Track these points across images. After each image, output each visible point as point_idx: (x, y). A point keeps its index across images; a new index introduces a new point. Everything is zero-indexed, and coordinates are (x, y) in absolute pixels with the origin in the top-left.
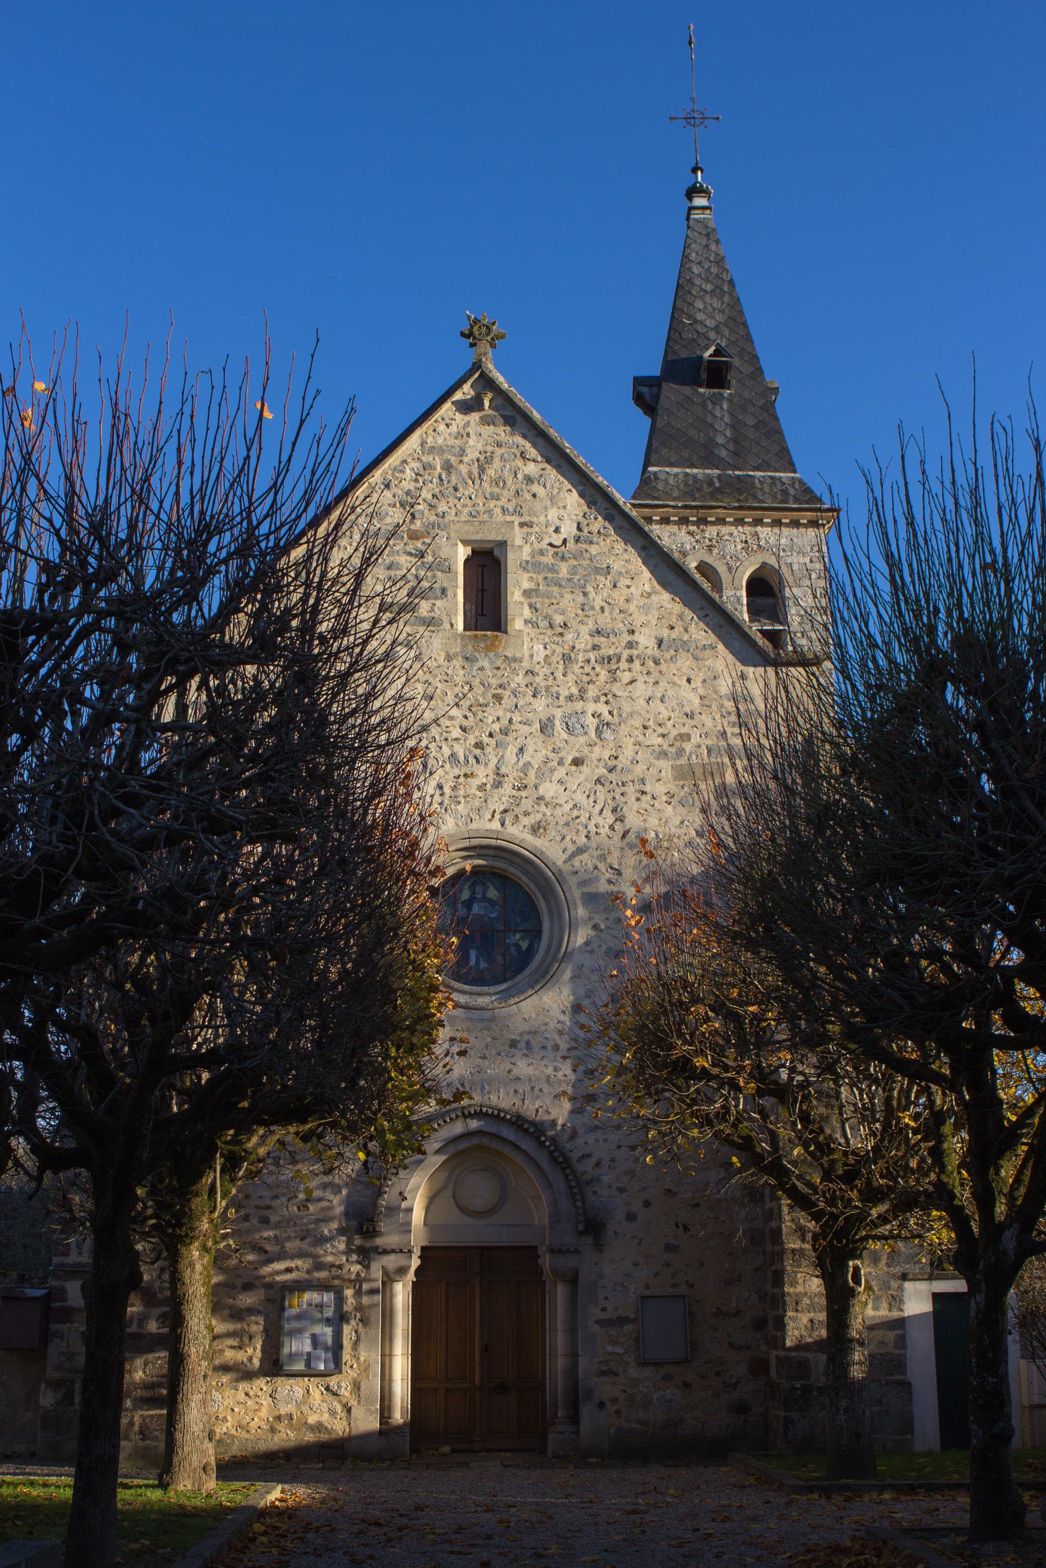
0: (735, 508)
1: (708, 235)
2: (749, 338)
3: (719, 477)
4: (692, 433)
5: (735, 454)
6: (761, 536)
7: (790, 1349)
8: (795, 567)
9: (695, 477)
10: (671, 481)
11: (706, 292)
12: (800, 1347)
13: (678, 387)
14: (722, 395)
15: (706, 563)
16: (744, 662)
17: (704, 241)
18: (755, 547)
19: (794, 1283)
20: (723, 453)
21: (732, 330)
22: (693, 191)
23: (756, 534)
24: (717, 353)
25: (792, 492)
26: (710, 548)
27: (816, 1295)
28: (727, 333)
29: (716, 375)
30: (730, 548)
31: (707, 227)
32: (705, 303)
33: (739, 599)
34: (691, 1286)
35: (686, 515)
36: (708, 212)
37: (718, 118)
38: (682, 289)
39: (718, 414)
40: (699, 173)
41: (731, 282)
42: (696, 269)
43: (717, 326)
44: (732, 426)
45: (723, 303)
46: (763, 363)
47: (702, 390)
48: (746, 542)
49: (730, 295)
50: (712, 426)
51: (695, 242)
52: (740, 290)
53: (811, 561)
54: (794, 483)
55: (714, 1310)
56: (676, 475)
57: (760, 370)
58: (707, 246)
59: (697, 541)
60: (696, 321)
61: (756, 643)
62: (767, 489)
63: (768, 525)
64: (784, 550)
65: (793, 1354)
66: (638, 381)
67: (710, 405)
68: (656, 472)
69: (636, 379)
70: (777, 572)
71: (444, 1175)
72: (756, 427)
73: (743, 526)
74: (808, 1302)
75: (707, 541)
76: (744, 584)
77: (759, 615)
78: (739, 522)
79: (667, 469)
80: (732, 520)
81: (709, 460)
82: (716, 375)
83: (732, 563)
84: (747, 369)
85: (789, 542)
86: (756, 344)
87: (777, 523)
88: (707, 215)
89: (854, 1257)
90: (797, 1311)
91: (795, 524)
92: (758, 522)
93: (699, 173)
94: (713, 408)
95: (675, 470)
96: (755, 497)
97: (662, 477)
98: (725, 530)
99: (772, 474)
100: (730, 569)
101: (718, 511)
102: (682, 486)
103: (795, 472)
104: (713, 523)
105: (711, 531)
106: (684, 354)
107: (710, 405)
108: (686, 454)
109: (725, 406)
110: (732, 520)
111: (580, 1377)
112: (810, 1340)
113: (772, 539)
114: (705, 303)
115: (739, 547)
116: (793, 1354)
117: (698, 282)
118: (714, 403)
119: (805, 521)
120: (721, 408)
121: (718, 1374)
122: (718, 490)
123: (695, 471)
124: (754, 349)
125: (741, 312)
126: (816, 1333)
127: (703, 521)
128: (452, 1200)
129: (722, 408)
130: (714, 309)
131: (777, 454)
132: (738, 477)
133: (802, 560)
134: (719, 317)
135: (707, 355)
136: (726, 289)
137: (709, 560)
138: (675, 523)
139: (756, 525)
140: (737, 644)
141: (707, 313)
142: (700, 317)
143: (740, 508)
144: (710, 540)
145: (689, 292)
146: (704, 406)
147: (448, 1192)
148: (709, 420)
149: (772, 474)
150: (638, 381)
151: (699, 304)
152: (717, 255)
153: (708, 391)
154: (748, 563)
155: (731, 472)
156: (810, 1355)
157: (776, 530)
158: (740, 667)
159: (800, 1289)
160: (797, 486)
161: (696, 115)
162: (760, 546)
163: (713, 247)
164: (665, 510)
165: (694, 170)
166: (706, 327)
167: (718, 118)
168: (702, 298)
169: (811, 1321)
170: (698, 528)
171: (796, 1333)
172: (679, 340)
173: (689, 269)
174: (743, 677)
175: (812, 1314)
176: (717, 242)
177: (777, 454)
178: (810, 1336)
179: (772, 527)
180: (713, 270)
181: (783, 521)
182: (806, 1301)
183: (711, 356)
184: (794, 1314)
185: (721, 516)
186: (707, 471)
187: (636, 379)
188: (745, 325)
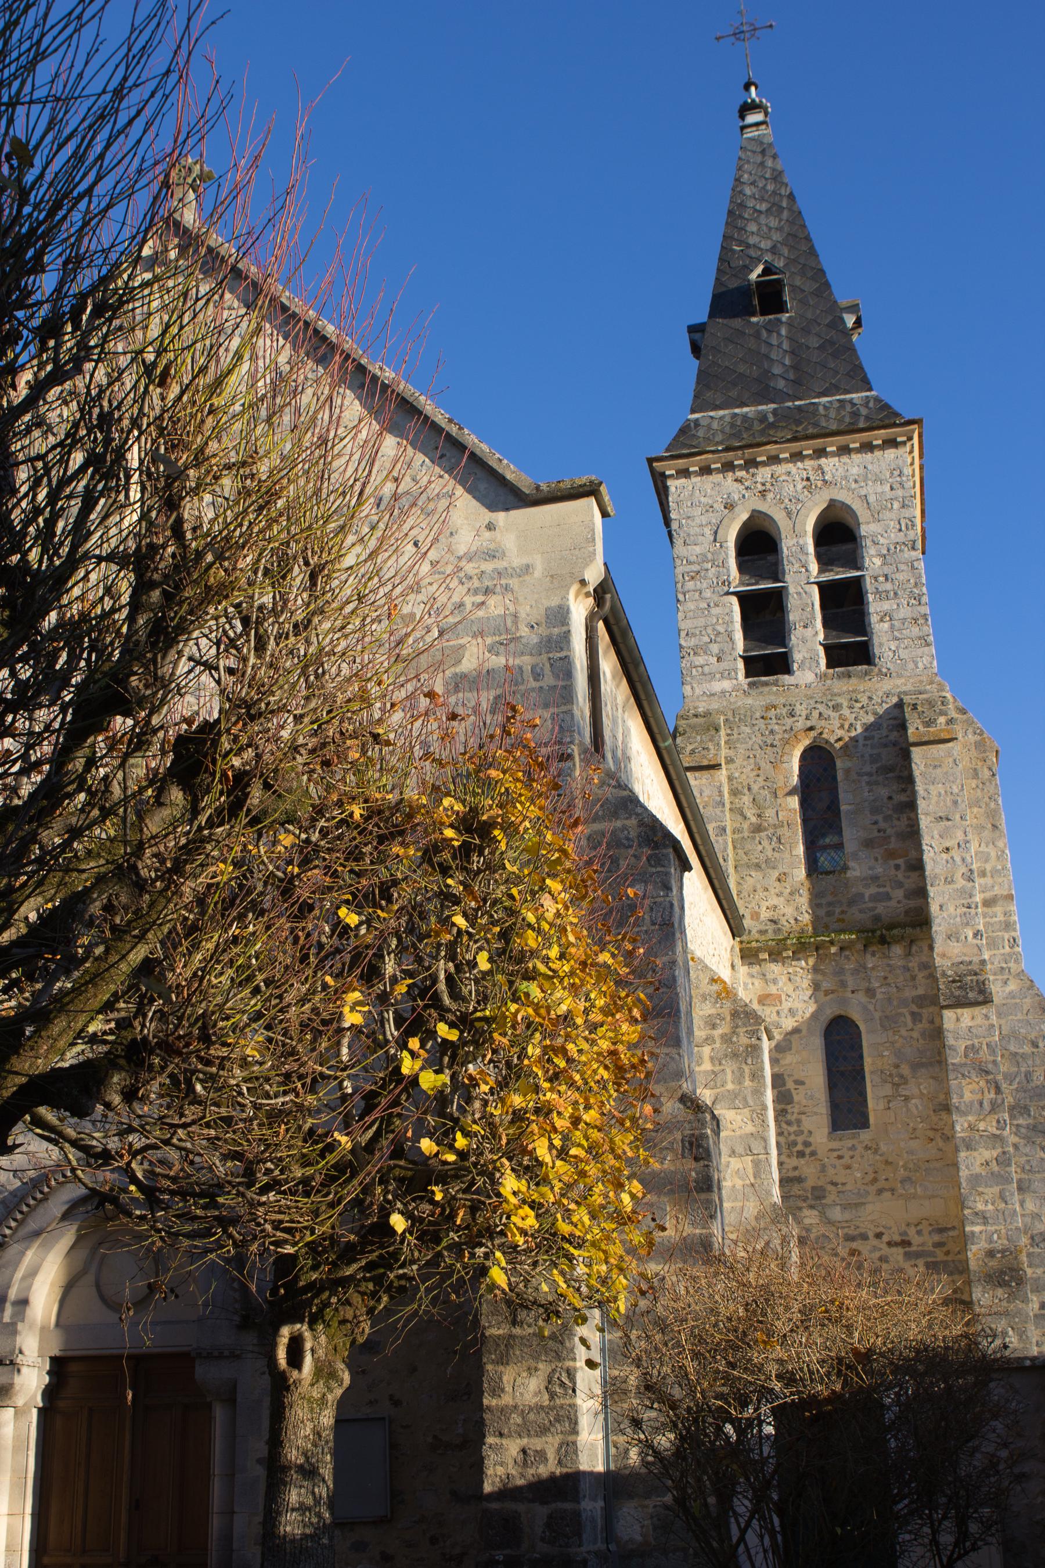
0: (789, 441)
1: (763, 152)
2: (812, 252)
3: (775, 412)
4: (742, 368)
5: (797, 382)
6: (826, 469)
7: (491, 1497)
8: (872, 499)
9: (745, 417)
10: (715, 425)
11: (760, 212)
12: (507, 1493)
13: (725, 321)
14: (779, 320)
15: (760, 512)
16: (492, 507)
17: (759, 159)
18: (819, 484)
19: (498, 1390)
20: (781, 384)
21: (792, 248)
22: (747, 108)
23: (820, 467)
24: (766, 271)
25: (864, 411)
26: (763, 493)
27: (531, 1409)
28: (785, 251)
29: (770, 297)
30: (788, 490)
31: (762, 143)
32: (759, 224)
33: (802, 549)
34: (396, 1403)
35: (729, 459)
36: (763, 127)
37: (771, 26)
38: (735, 216)
39: (775, 342)
40: (753, 89)
41: (791, 197)
42: (748, 191)
43: (774, 247)
44: (792, 352)
45: (780, 220)
46: (830, 277)
47: (754, 319)
48: (808, 479)
49: (790, 210)
50: (767, 357)
51: (748, 162)
52: (802, 203)
53: (892, 489)
54: (868, 403)
55: (430, 1440)
56: (722, 418)
57: (827, 285)
58: (762, 164)
59: (747, 488)
60: (748, 246)
61: (504, 478)
62: (832, 414)
63: (833, 454)
64: (856, 481)
65: (494, 1506)
66: (692, 329)
67: (764, 334)
68: (697, 420)
69: (689, 327)
70: (848, 508)
71: (82, 1254)
72: (821, 348)
73: (802, 461)
74: (519, 1420)
75: (759, 486)
76: (810, 527)
77: (832, 564)
78: (797, 457)
79: (712, 414)
80: (787, 455)
81: (764, 395)
82: (770, 297)
83: (792, 507)
84: (810, 286)
85: (862, 471)
86: (822, 258)
87: (844, 450)
88: (763, 130)
89: (295, 1317)
90: (501, 1435)
91: (867, 447)
92: (820, 453)
93: (753, 89)
94: (769, 337)
95: (721, 413)
96: (816, 425)
97: (703, 423)
98: (780, 469)
99: (842, 397)
100: (789, 514)
101: (768, 447)
102: (727, 429)
103: (870, 389)
104: (764, 464)
105: (764, 474)
106: (733, 284)
107: (764, 334)
108: (734, 393)
109: (783, 332)
110: (787, 455)
111: (235, 1546)
112: (520, 1482)
113: (840, 470)
114: (759, 224)
115: (799, 487)
116: (494, 1506)
117: (751, 203)
118: (769, 331)
119: (880, 442)
120: (778, 336)
121: (434, 1540)
122: (772, 426)
123: (745, 409)
124: (819, 262)
125: (804, 226)
126: (531, 1471)
127: (751, 464)
128: (94, 1289)
129: (779, 334)
130: (770, 229)
131: (848, 374)
132: (799, 408)
133: (879, 489)
134: (776, 236)
135: (753, 276)
136: (784, 204)
137: (763, 507)
138: (717, 470)
139: (819, 457)
140: (482, 486)
141: (762, 235)
142: (752, 240)
143: (795, 439)
144: (763, 484)
145: (741, 217)
146: (757, 336)
147: (90, 1278)
148: (764, 350)
149: (842, 397)
150: (692, 329)
151: (752, 227)
152: (774, 170)
153: (762, 318)
154: (811, 503)
155: (790, 404)
156: (521, 1508)
157: (845, 459)
158: (487, 516)
159: (507, 1400)
160: (871, 405)
161: (745, 28)
162: (825, 482)
163: (769, 163)
164: (703, 457)
165: (747, 87)
166: (760, 249)
167: (771, 26)
168: (755, 220)
169: (524, 1451)
170: (748, 472)
171: (500, 1470)
172: (728, 270)
173: (740, 192)
174: (490, 527)
175: (525, 1441)
176: (775, 157)
177: (848, 374)
178: (522, 1475)
179: (839, 456)
180: (769, 187)
181: (852, 446)
182: (516, 1419)
183: (759, 276)
184: (497, 1440)
185: (773, 453)
186: (760, 408)
187: (689, 327)
188: (808, 239)
